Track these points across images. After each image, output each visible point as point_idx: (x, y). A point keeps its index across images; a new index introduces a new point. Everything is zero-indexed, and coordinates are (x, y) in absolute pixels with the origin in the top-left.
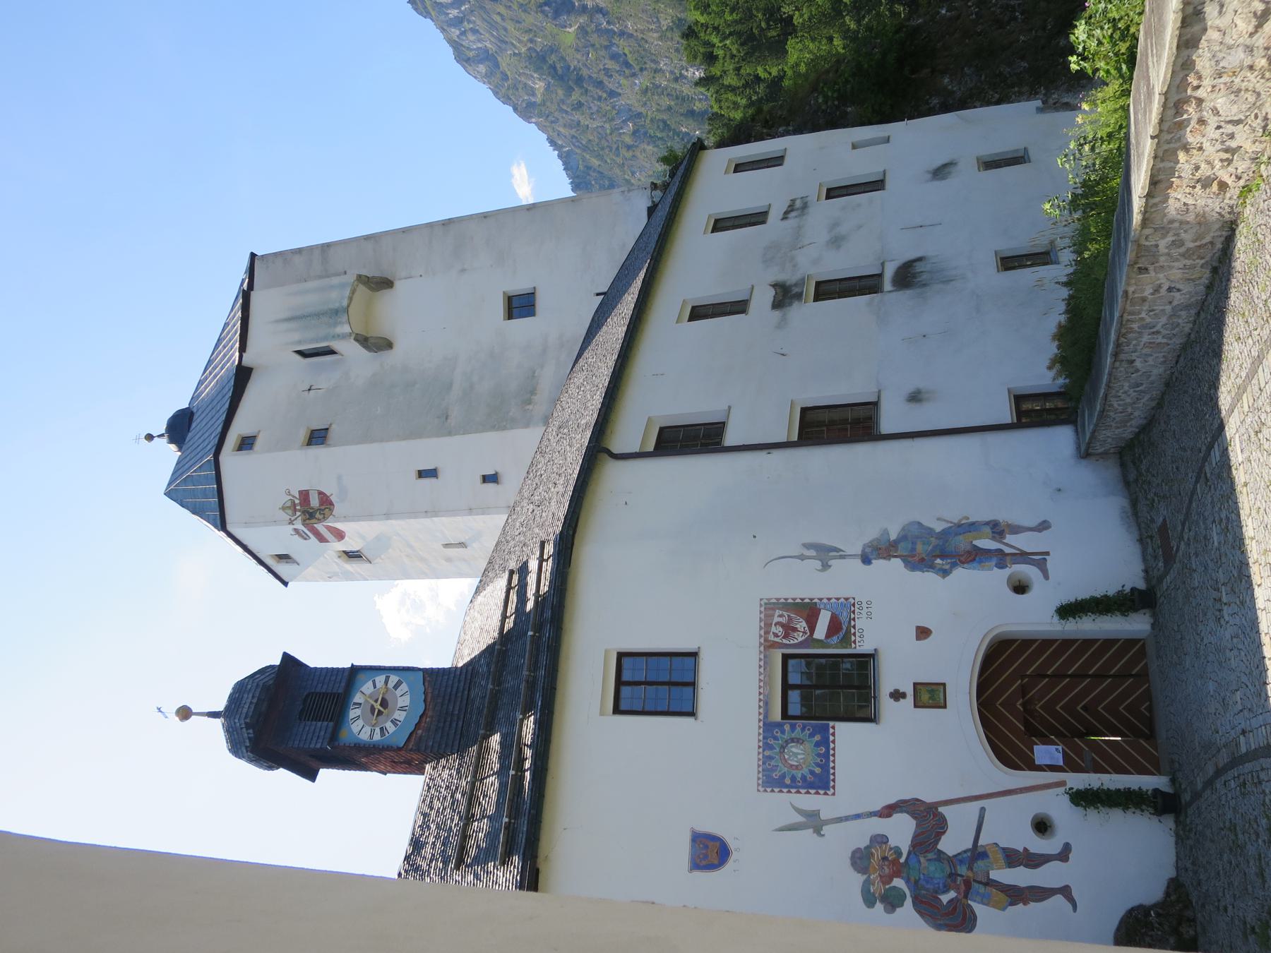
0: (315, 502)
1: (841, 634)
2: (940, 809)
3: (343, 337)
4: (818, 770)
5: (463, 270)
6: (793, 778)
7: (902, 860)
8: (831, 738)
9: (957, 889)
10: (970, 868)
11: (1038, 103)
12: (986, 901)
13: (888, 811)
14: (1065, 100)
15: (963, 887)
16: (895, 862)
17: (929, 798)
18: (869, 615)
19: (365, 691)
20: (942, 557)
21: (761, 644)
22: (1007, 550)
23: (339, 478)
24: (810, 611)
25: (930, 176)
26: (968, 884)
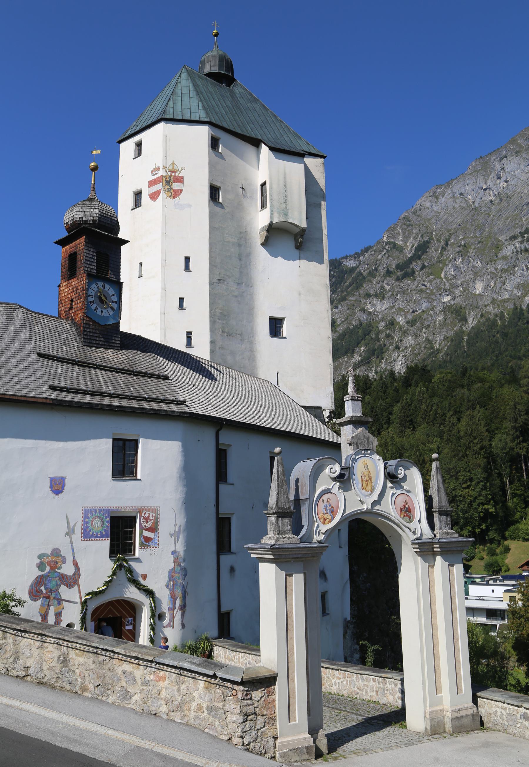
0: (176, 186)
1: (144, 542)
2: (76, 585)
3: (272, 214)
4: (91, 533)
5: (300, 294)
6: (87, 523)
7: (56, 570)
8: (104, 539)
9: (46, 593)
10: (54, 598)
11: (349, 619)
12: (42, 605)
13: (76, 564)
14: (348, 632)
15: (47, 595)
16: (56, 567)
17: (81, 581)
18: (151, 554)
19: (110, 290)
20: (174, 584)
21: (141, 507)
22: (175, 611)
23: (190, 206)
24: (153, 529)
25: (322, 569)
26: (48, 597)
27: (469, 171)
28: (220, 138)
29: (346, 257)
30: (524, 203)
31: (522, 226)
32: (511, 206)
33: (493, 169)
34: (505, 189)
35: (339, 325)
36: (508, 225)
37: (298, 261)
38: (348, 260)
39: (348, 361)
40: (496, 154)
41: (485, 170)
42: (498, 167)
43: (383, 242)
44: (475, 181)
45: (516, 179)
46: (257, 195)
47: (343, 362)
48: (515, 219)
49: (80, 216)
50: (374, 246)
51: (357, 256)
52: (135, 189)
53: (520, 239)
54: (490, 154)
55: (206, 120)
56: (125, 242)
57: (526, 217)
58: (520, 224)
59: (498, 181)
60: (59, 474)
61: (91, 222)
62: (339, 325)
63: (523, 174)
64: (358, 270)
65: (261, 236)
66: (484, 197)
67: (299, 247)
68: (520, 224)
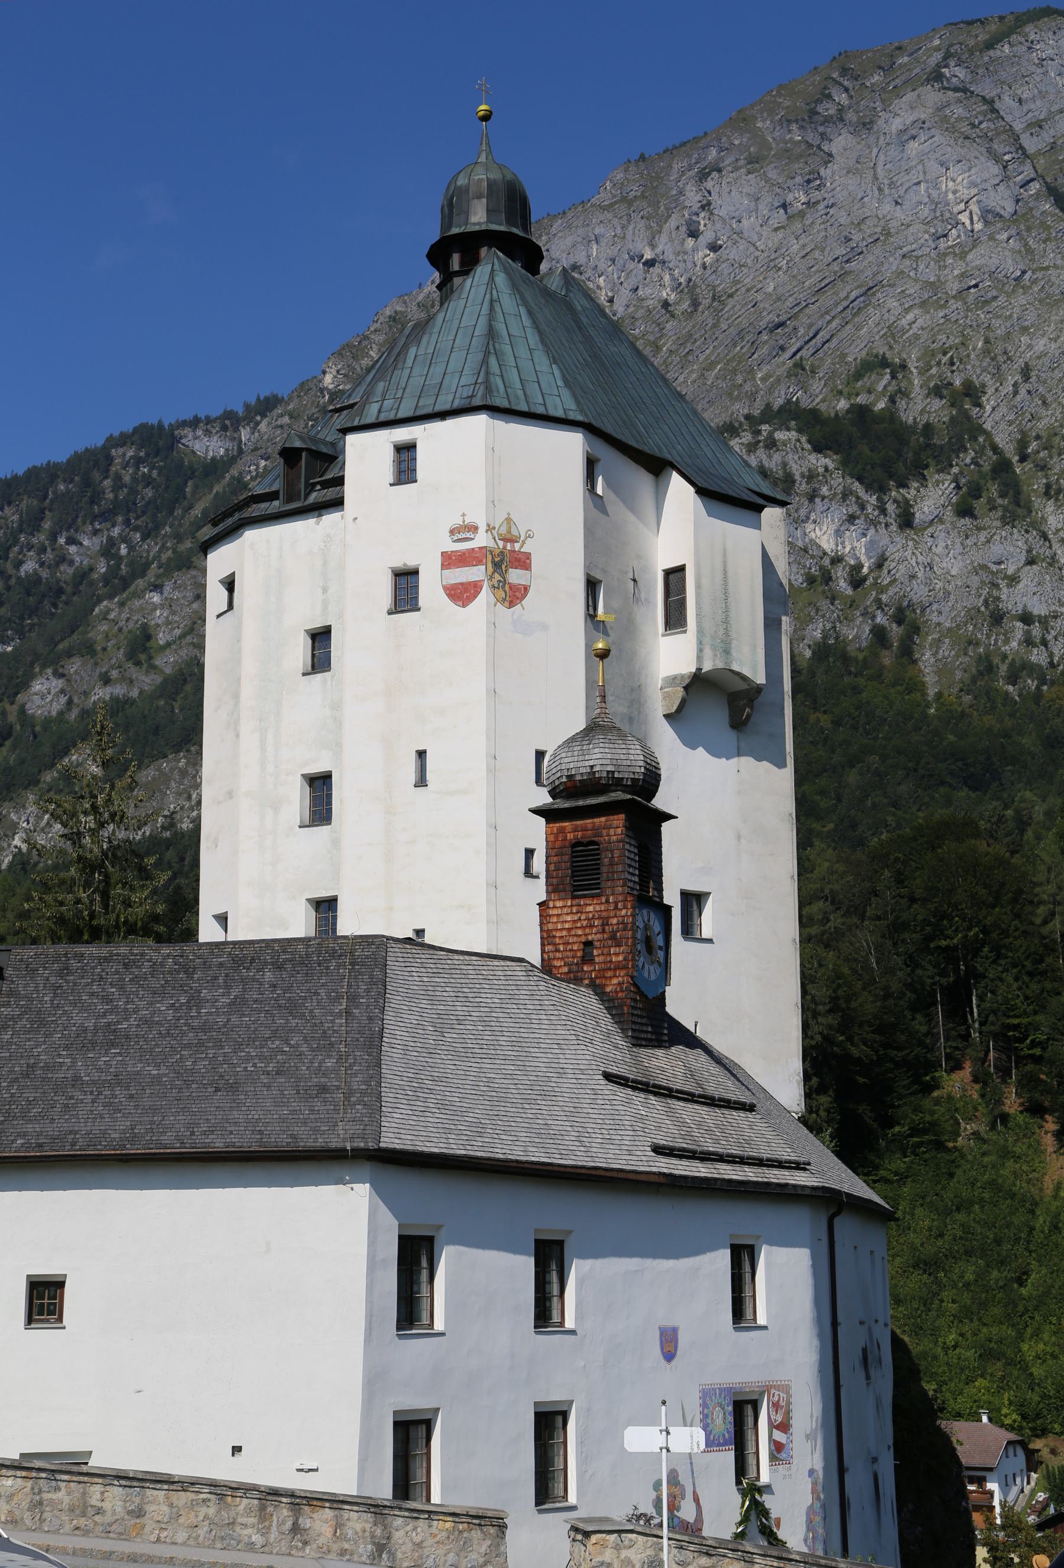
0: (515, 576)
23: (545, 627)
27: (604, 197)
28: (599, 460)
29: (194, 423)
30: (763, 324)
31: (752, 397)
32: (724, 326)
33: (677, 202)
34: (708, 272)
35: (163, 648)
36: (712, 386)
37: (735, 760)
38: (199, 433)
39: (190, 770)
40: (689, 156)
41: (651, 200)
42: (692, 197)
43: (322, 390)
44: (619, 231)
45: (742, 245)
46: (656, 594)
47: (172, 770)
48: (734, 372)
49: (609, 768)
50: (291, 398)
51: (229, 422)
52: (398, 563)
53: (747, 437)
54: (670, 152)
55: (579, 418)
56: (669, 817)
57: (766, 368)
58: (747, 387)
59: (690, 242)
60: (670, 1323)
61: (629, 783)
62: (163, 648)
63: (765, 232)
64: (234, 472)
65: (666, 696)
66: (645, 285)
67: (738, 723)
68: (747, 387)
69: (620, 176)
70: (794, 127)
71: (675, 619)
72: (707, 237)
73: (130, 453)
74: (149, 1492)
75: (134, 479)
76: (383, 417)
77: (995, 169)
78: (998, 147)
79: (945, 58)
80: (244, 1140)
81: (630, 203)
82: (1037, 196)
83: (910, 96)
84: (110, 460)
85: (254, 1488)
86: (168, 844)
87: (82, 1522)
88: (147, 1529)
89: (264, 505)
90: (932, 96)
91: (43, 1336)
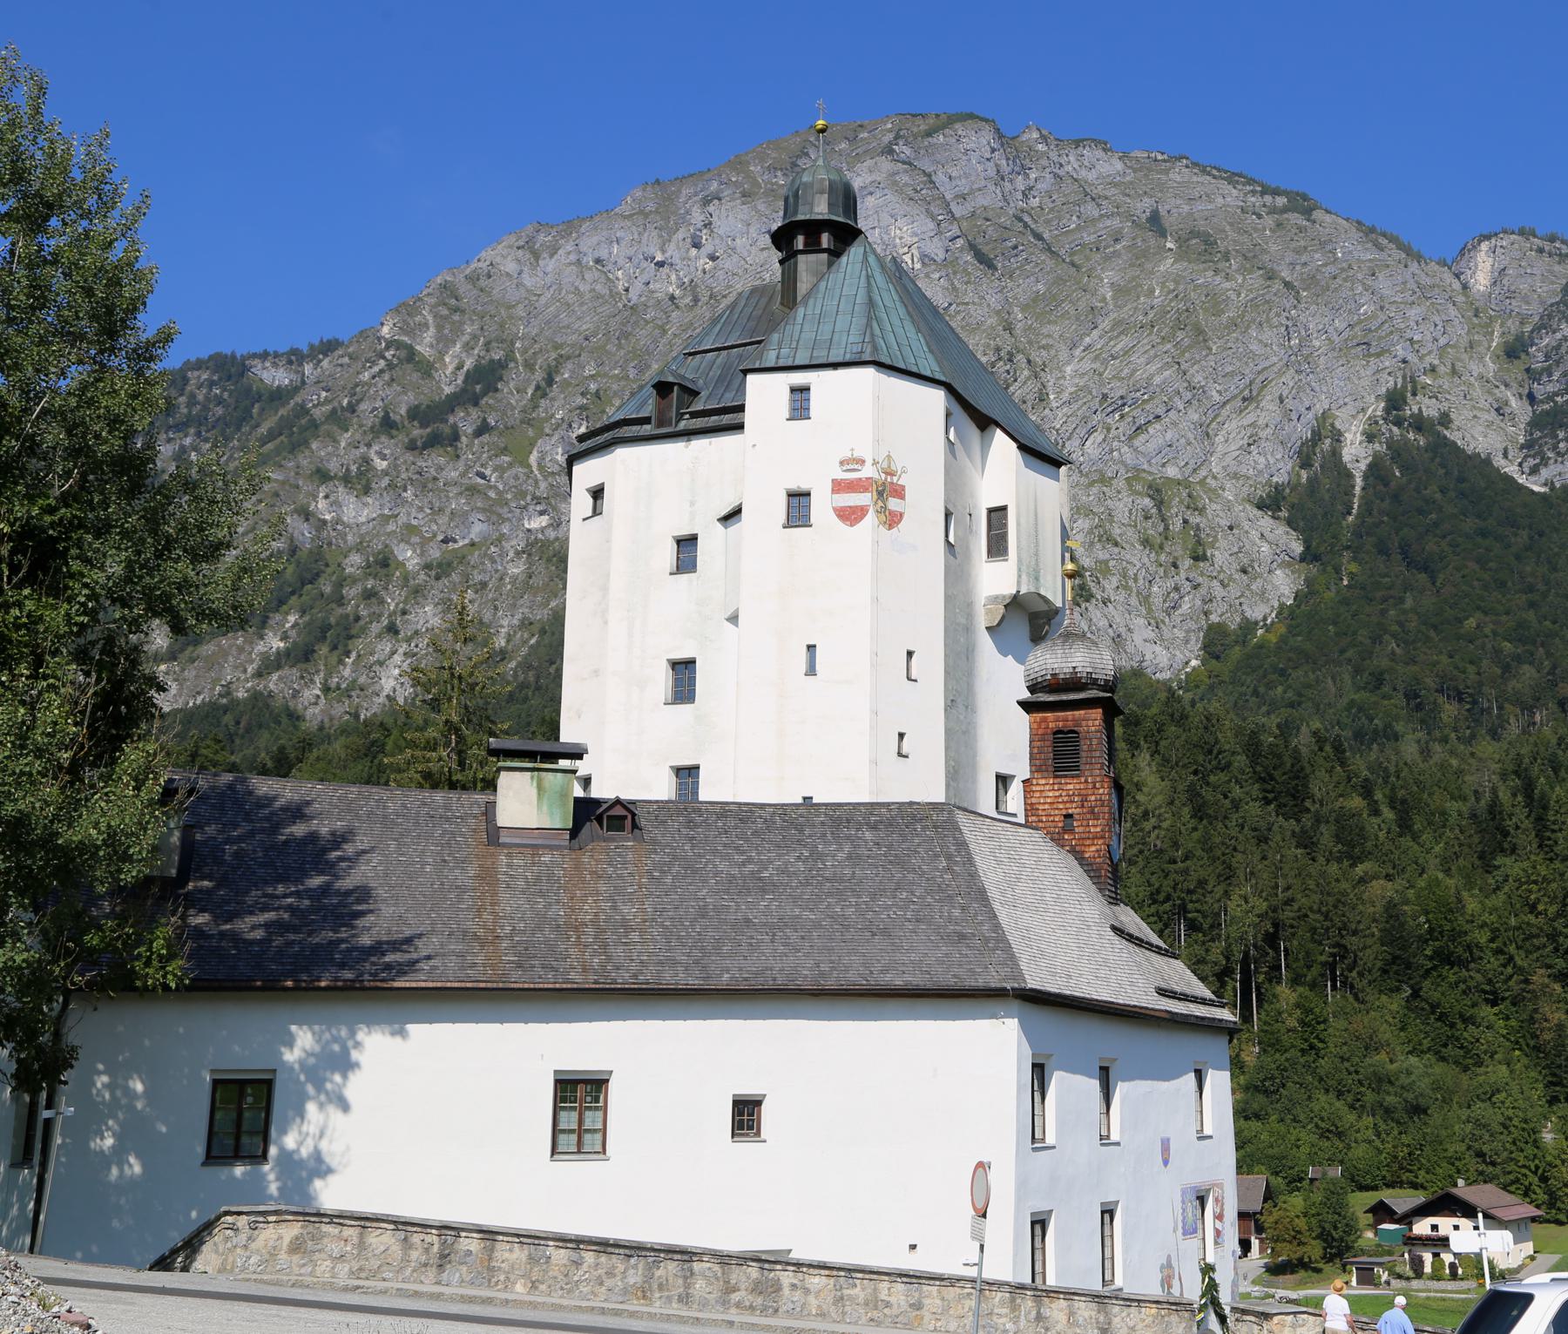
0: (893, 504)
29: (264, 356)
33: (684, 219)
38: (268, 364)
39: (247, 648)
41: (665, 217)
42: (697, 217)
43: (379, 339)
45: (735, 258)
47: (231, 646)
50: (351, 342)
51: (294, 358)
52: (794, 486)
55: (943, 378)
59: (694, 252)
63: (754, 250)
64: (298, 399)
65: (988, 612)
69: (638, 193)
70: (779, 173)
71: (997, 547)
72: (708, 248)
73: (205, 376)
74: (925, 1288)
75: (207, 398)
76: (781, 363)
77: (932, 225)
78: (935, 210)
79: (896, 138)
80: (854, 976)
81: (646, 215)
82: (961, 249)
83: (869, 163)
84: (186, 380)
85: (1008, 1284)
86: (226, 709)
87: (875, 1314)
88: (926, 1320)
89: (635, 428)
90: (885, 164)
91: (746, 1148)
